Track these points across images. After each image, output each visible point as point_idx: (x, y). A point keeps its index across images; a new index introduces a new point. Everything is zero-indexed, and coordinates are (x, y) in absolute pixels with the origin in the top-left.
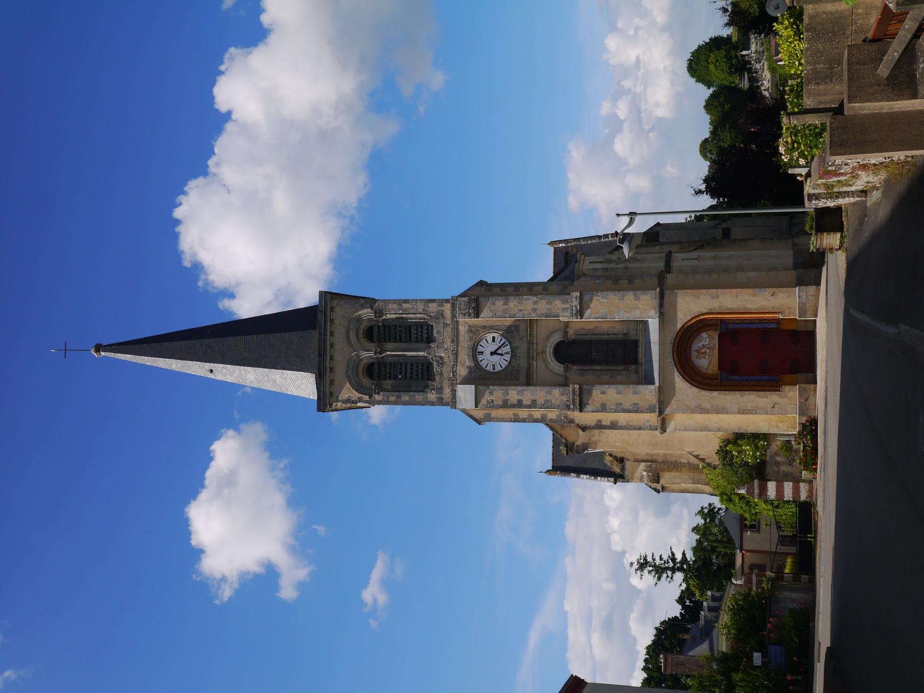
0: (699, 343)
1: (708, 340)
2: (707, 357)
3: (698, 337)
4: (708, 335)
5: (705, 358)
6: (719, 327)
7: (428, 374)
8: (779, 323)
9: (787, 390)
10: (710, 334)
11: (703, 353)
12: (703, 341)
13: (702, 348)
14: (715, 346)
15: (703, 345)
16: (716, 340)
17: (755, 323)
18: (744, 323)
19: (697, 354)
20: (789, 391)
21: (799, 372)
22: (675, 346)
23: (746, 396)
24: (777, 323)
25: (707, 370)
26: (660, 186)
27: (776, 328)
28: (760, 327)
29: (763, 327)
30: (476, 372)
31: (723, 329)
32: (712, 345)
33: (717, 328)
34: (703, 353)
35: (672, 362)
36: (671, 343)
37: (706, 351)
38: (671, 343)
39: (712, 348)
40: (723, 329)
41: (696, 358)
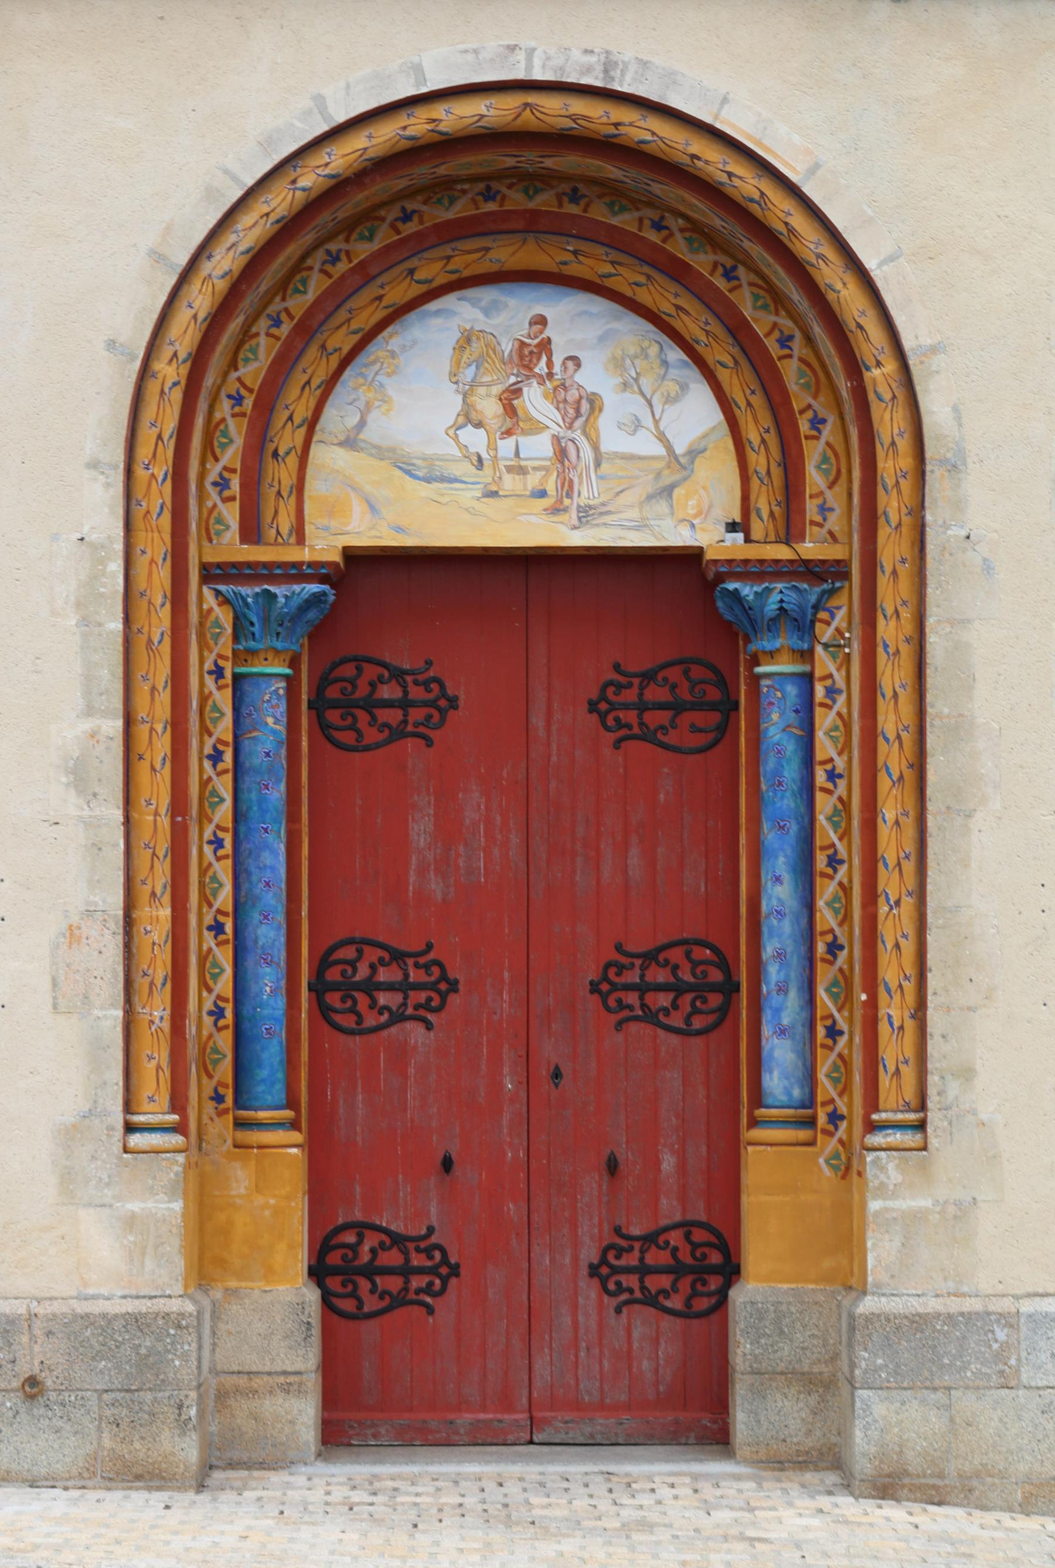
0: (618, 364)
1: (646, 445)
2: (475, 439)
3: (675, 354)
4: (694, 453)
5: (469, 418)
6: (782, 553)
7: (1013, 1296)
8: (811, 1122)
9: (135, 1206)
10: (702, 470)
11: (510, 399)
12: (635, 404)
13: (558, 393)
14: (586, 515)
15: (595, 402)
16: (641, 526)
17: (809, 906)
18: (808, 789)
19: (507, 347)
20: (130, 1222)
21: (326, 1301)
22: (579, 106)
23: (73, 806)
24: (810, 1102)
25: (350, 443)
26: (533, 1523)
27: (757, 1098)
28: (769, 950)
29: (773, 973)
30: (1047, 1436)
31: (748, 591)
32: (588, 492)
33: (758, 529)
34: (510, 399)
35: (418, 70)
36: (608, 67)
37: (537, 428)
38: (608, 67)
39: (568, 488)
40: (748, 591)
41: (467, 339)
